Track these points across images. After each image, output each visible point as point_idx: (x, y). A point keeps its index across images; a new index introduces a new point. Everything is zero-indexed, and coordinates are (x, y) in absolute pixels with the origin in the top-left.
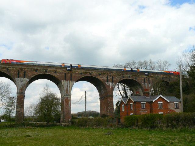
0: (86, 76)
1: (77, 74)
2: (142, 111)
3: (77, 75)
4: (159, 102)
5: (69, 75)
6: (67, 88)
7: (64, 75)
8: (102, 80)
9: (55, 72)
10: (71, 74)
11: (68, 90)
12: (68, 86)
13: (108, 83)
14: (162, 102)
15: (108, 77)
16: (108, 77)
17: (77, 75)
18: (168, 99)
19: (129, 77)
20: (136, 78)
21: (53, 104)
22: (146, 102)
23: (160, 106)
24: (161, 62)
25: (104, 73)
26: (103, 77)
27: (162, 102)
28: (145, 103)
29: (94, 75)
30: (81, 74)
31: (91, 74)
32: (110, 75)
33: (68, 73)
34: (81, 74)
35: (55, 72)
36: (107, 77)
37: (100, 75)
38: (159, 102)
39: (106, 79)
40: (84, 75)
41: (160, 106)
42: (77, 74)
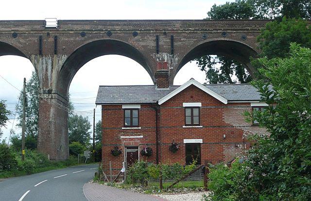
0: (96, 39)
1: (72, 36)
2: (126, 133)
3: (72, 39)
4: (185, 105)
5: (51, 39)
6: (46, 74)
7: (36, 40)
8: (141, 50)
9: (15, 35)
10: (56, 37)
11: (47, 79)
12: (47, 70)
13: (159, 55)
14: (199, 104)
15: (157, 40)
16: (157, 40)
17: (72, 39)
18: (221, 94)
19: (224, 34)
20: (244, 38)
21: (237, 191)
22: (142, 105)
23: (192, 116)
24: (229, 3)
25: (148, 28)
26: (143, 40)
27: (199, 104)
28: (139, 107)
29: (119, 37)
30: (83, 35)
31: (109, 34)
32: (165, 34)
33: (48, 34)
34: (83, 35)
35: (15, 35)
36: (155, 38)
37: (135, 34)
38: (185, 105)
39: (153, 44)
40: (91, 38)
41: (192, 116)
42: (73, 36)
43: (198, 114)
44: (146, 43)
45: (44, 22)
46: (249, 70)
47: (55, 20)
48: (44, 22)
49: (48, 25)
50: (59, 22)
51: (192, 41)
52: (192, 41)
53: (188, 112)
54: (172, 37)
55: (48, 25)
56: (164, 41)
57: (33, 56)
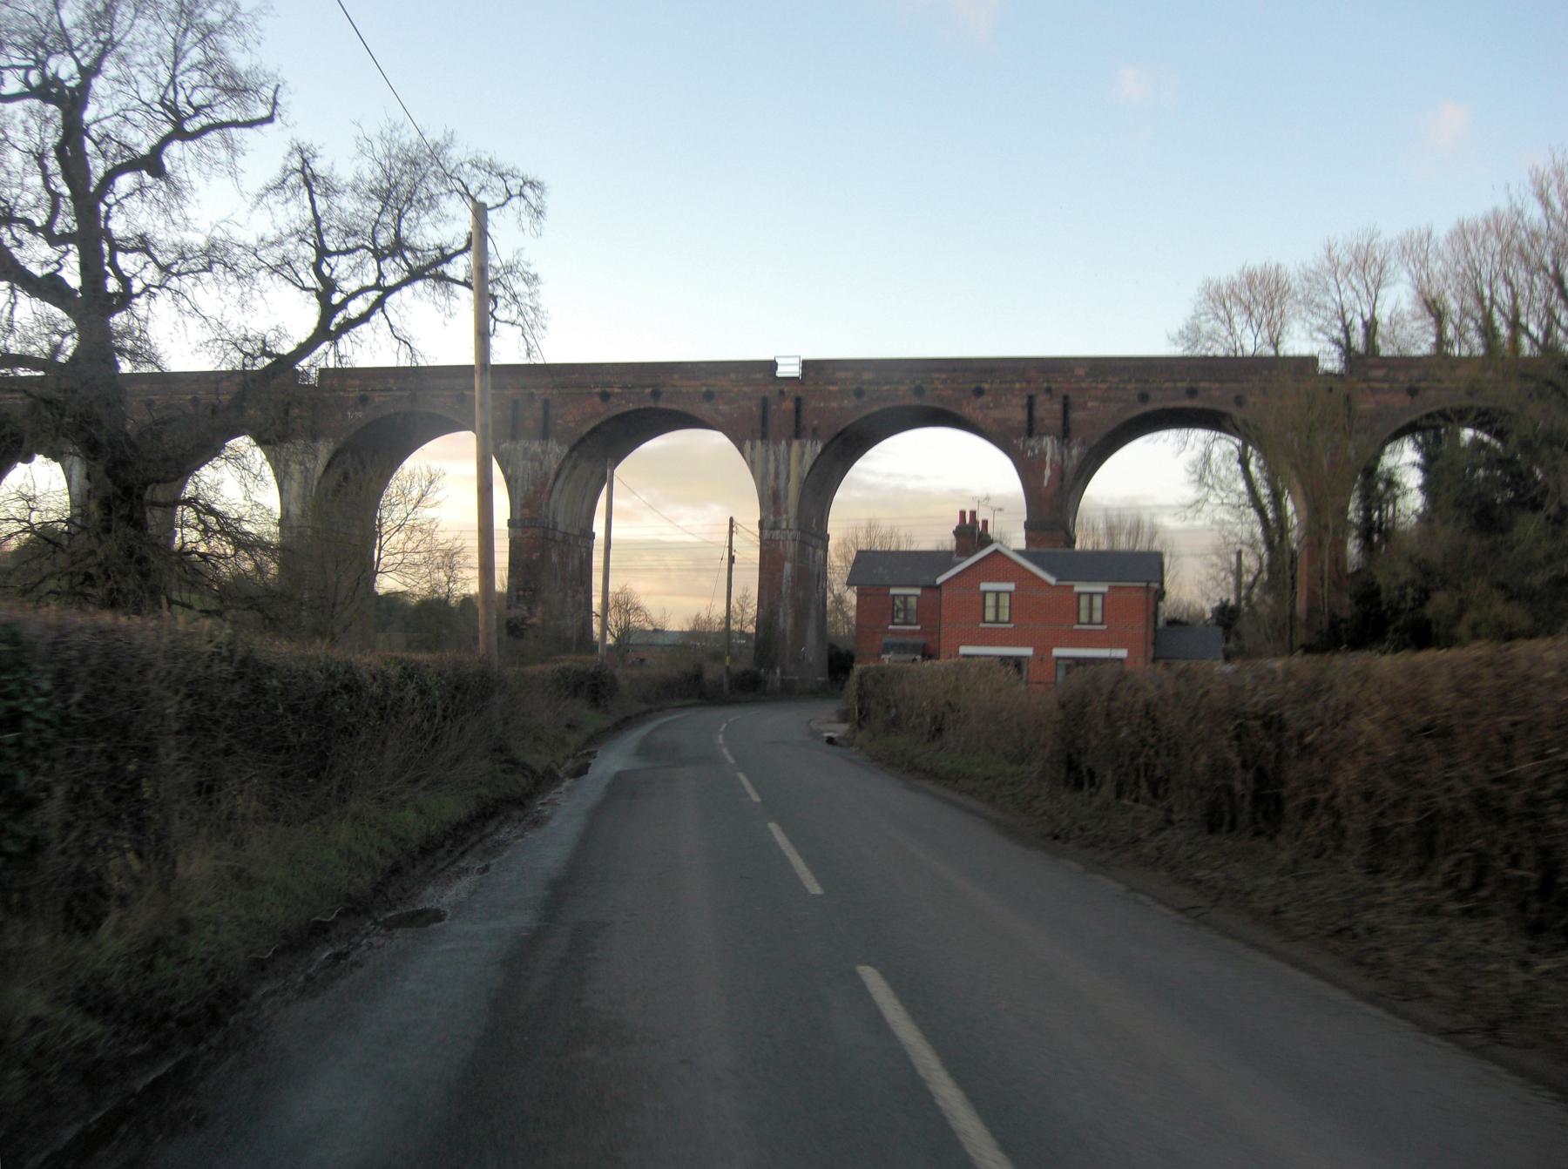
4: (984, 586)
5: (789, 405)
9: (709, 396)
15: (1030, 406)
16: (1030, 406)
32: (1049, 390)
33: (782, 392)
36: (1025, 401)
37: (979, 392)
38: (984, 586)
43: (1007, 604)
44: (1213, 395)
45: (772, 365)
46: (1376, 489)
47: (797, 361)
48: (772, 365)
49: (782, 372)
50: (807, 365)
51: (406, 472)
52: (406, 472)
53: (990, 600)
54: (1066, 398)
55: (782, 372)
56: (1048, 410)
57: (748, 444)
